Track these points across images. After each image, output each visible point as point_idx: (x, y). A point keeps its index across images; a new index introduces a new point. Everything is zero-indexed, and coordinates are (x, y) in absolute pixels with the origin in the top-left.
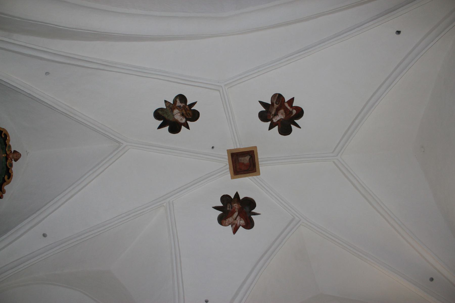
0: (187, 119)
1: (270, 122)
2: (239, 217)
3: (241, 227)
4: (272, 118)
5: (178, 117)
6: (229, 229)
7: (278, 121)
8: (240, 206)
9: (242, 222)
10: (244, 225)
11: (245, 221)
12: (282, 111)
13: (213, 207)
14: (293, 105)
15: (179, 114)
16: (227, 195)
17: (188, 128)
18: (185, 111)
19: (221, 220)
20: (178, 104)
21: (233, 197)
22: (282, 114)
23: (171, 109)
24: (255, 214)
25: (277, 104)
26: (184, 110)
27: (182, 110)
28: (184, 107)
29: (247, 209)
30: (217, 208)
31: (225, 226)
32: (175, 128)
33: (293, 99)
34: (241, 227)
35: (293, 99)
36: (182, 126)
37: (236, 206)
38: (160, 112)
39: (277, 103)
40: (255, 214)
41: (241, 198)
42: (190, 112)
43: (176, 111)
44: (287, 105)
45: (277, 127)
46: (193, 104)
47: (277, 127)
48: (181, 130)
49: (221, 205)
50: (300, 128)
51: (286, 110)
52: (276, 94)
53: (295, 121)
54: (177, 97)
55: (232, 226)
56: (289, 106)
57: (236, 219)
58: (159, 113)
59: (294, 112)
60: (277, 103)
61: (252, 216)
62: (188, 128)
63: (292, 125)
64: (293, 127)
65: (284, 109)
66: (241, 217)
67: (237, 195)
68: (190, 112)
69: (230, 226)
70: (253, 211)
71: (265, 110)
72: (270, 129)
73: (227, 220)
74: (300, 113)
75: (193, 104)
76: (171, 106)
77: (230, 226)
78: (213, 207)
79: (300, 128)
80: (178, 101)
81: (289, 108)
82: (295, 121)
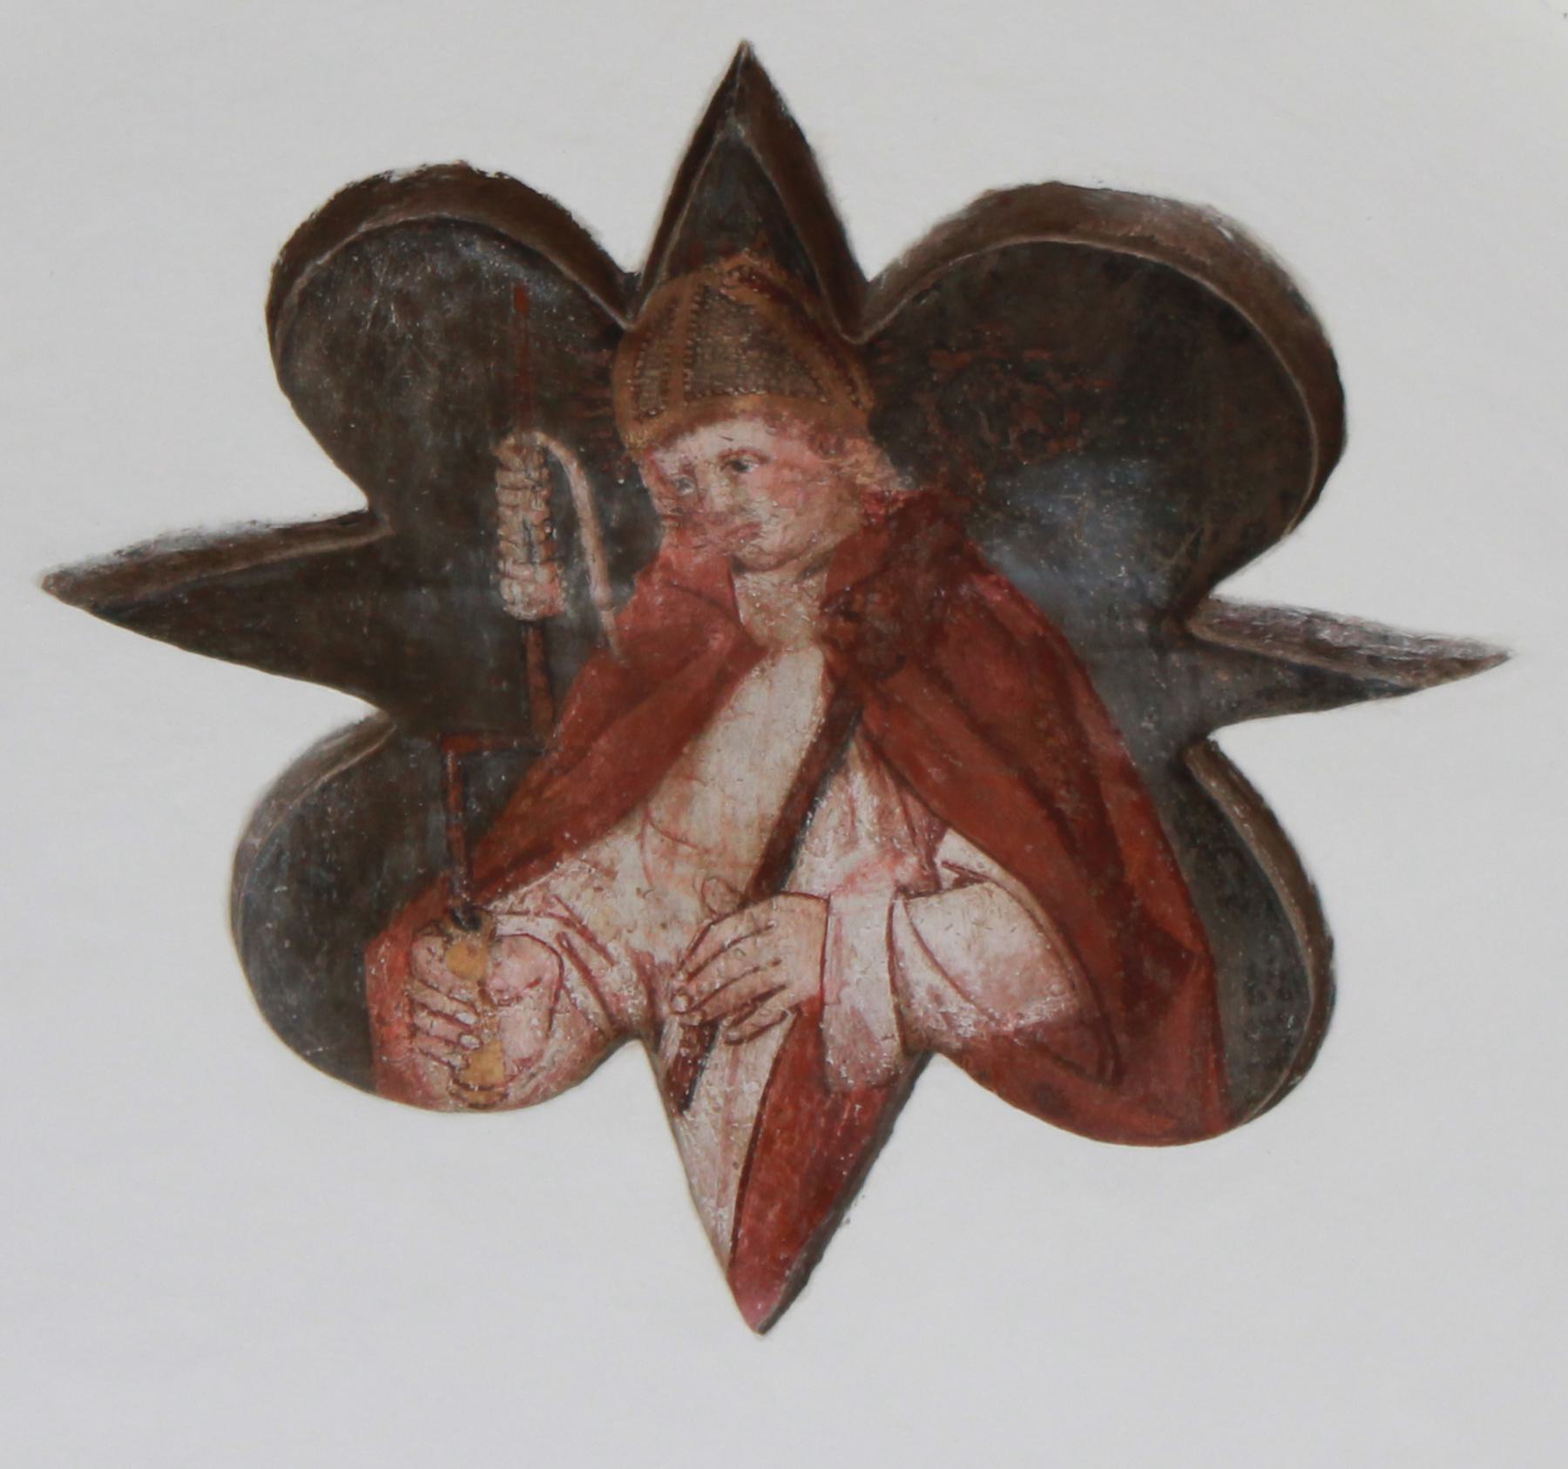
2: (858, 795)
3: (943, 1082)
6: (616, 1166)
8: (870, 467)
9: (985, 940)
10: (1045, 1002)
11: (1066, 930)
13: (74, 587)
16: (459, 184)
19: (346, 932)
21: (626, 230)
24: (1327, 669)
29: (1082, 546)
30: (190, 596)
31: (483, 1096)
34: (943, 1082)
37: (758, 482)
40: (1327, 669)
41: (880, 238)
49: (306, 485)
55: (678, 1090)
57: (774, 869)
61: (1271, 753)
66: (937, 796)
67: (750, 158)
69: (631, 1072)
70: (1256, 585)
73: (524, 915)
77: (631, 1072)
78: (74, 587)
82: (323, 712)
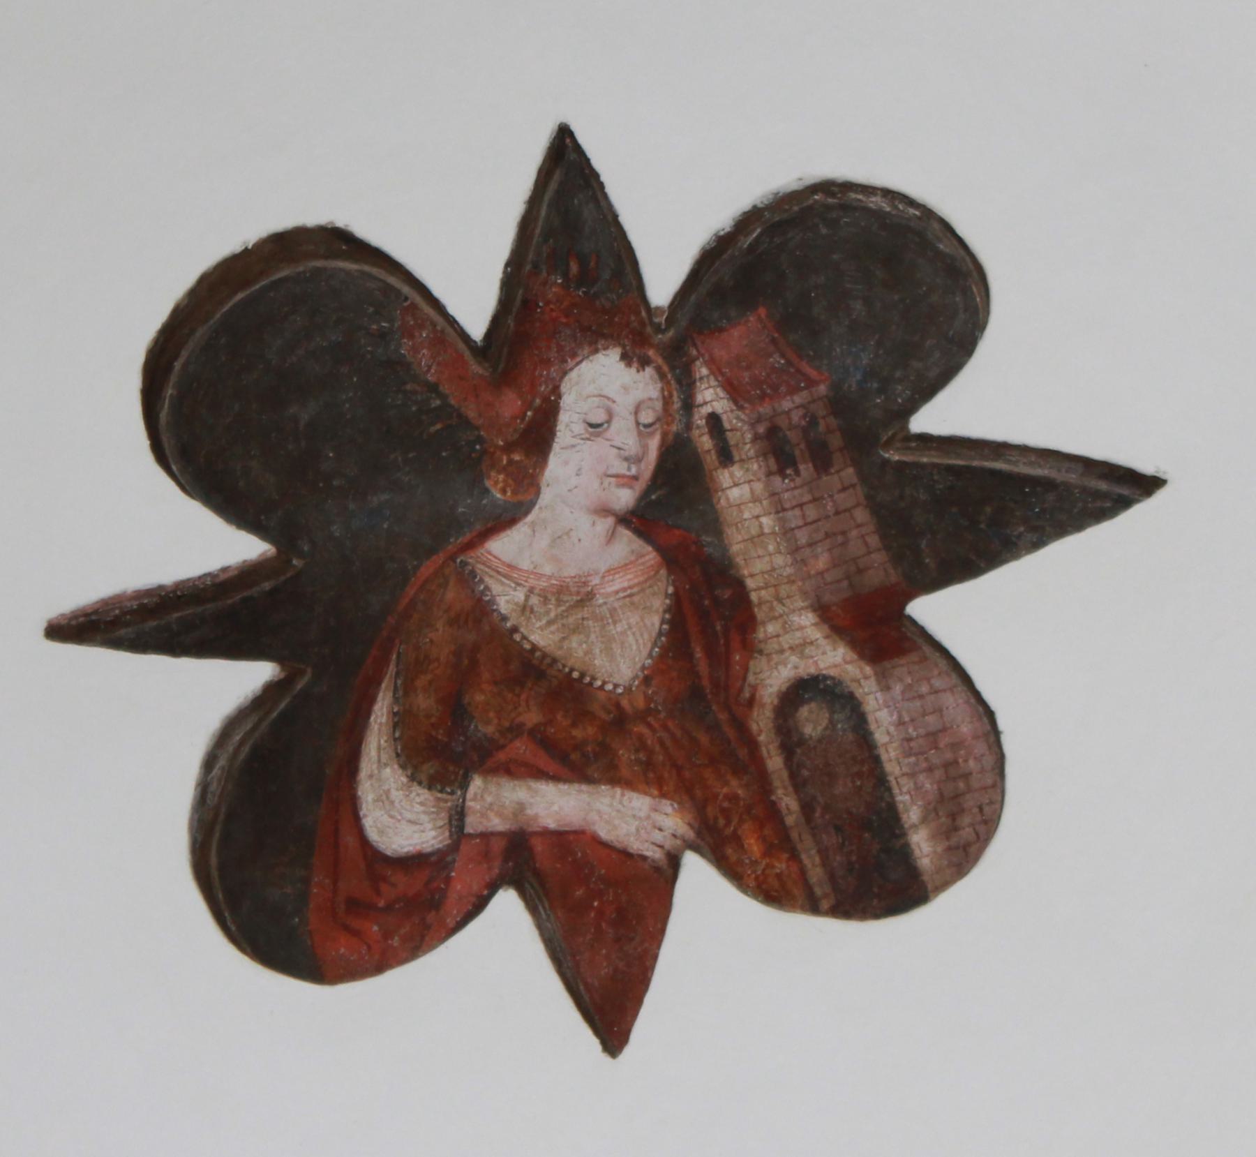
1: (663, 276)
4: (680, 380)
7: (538, 436)
12: (621, 650)
14: (507, 906)
22: (575, 597)
25: (807, 688)
33: (609, 1010)
35: (609, 1010)
39: (812, 721)
44: (630, 817)
45: (470, 293)
47: (472, 303)
50: (77, 629)
51: (575, 729)
52: (963, 856)
53: (250, 677)
56: (571, 843)
59: (398, 815)
60: (812, 721)
63: (236, 547)
64: (210, 545)
65: (619, 720)
71: (930, 419)
72: (566, 167)
74: (288, 875)
79: (77, 629)
81: (554, 804)
82: (250, 677)
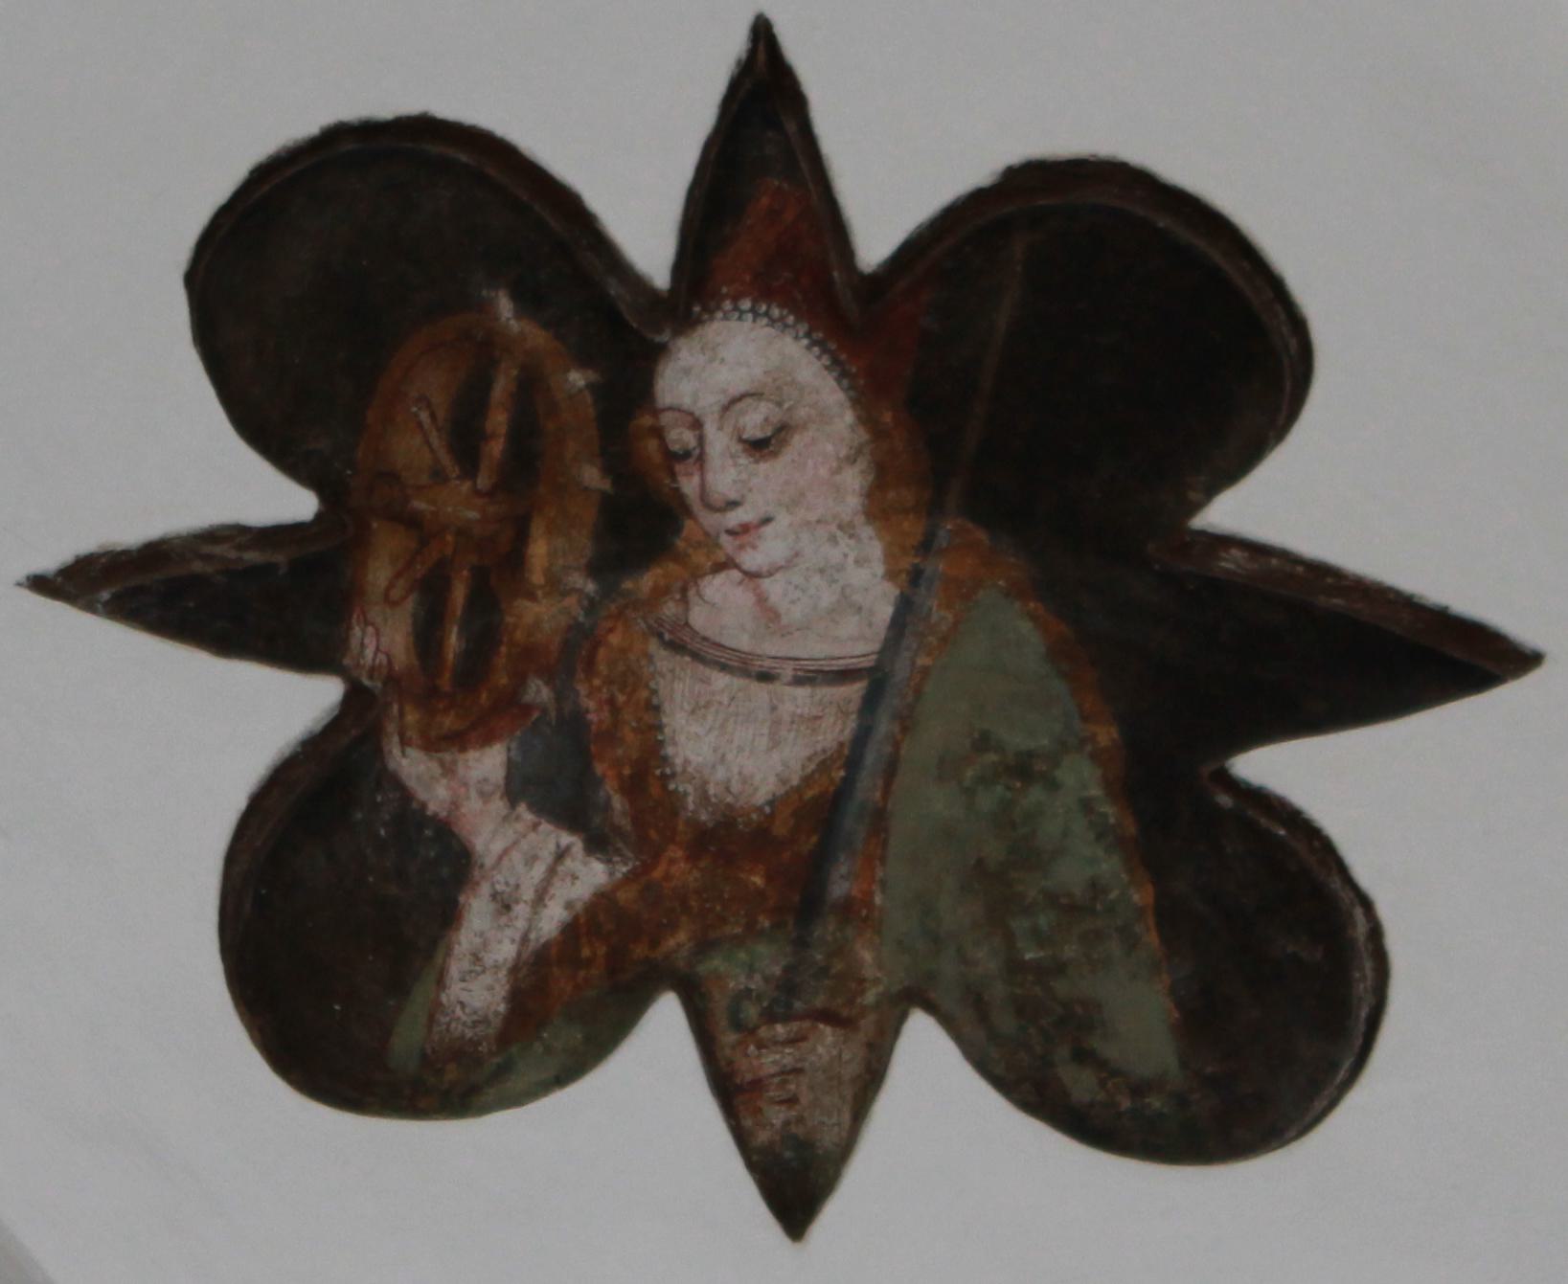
0: (626, 332)
5: (796, 565)
13: (40, 584)
15: (721, 607)
17: (764, 99)
18: (500, 570)
20: (528, 881)
23: (803, 902)
26: (539, 615)
27: (577, 650)
28: (462, 689)
32: (1092, 348)
36: (875, 242)
38: (1141, 1021)
42: (415, 443)
43: (736, 746)
46: (168, 588)
48: (974, 168)
54: (446, 1084)
58: (1200, 1019)
62: (764, 99)
68: (415, 443)
75: (168, 588)
76: (746, 969)
80: (478, 967)
